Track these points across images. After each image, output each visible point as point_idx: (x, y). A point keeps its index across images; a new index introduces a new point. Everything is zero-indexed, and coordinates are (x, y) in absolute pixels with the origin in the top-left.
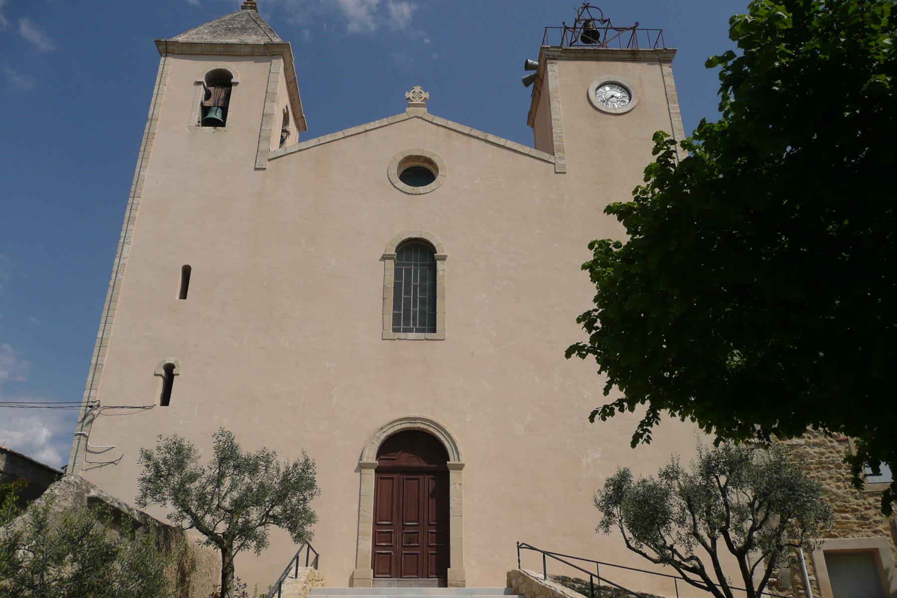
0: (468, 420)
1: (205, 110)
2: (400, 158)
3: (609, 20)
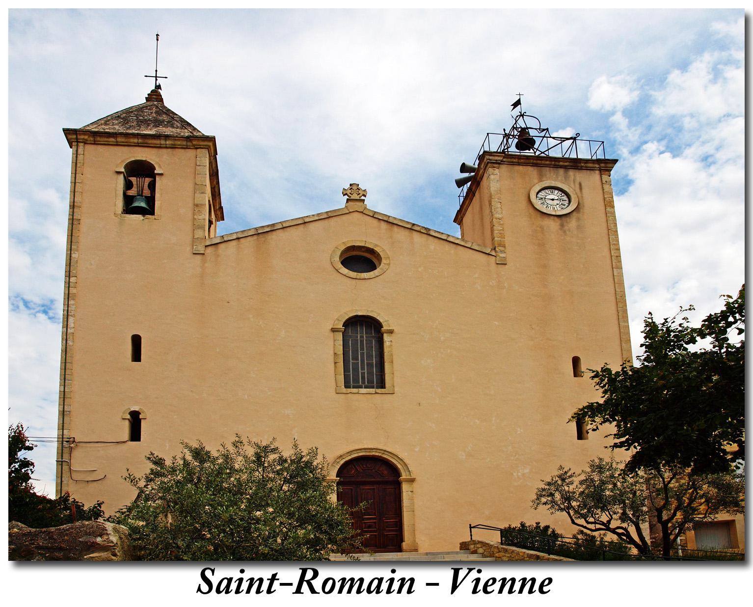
0: (417, 450)
1: (128, 200)
2: (343, 248)
3: (547, 129)
